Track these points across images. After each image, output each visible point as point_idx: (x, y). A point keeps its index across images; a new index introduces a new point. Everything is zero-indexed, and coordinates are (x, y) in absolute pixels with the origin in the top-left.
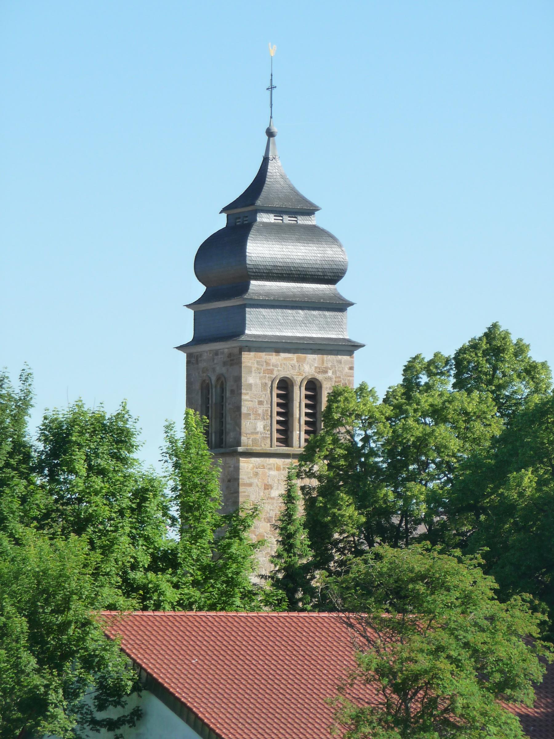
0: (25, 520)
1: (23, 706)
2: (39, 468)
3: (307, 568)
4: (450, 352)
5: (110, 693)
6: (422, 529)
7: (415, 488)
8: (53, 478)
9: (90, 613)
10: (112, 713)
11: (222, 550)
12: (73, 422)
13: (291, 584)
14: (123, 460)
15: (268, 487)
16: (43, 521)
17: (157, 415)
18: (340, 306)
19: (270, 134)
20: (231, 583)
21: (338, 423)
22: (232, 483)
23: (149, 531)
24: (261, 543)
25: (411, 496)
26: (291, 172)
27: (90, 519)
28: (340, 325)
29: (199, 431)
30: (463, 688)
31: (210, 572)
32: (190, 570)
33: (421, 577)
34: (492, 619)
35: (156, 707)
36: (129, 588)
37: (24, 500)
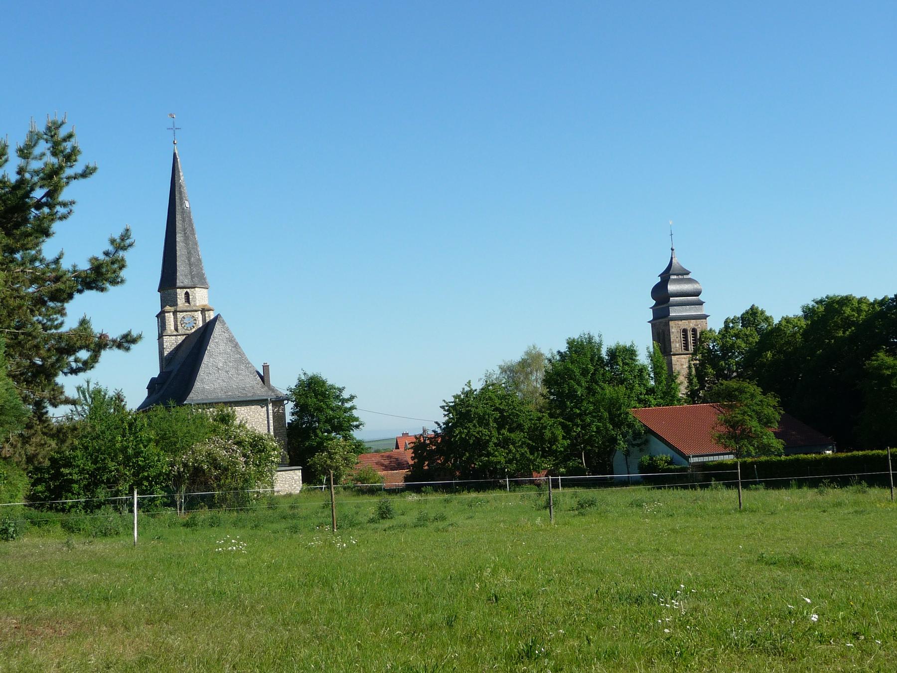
0: (604, 382)
2: (607, 365)
3: (698, 390)
4: (739, 315)
5: (637, 435)
6: (735, 374)
7: (732, 361)
8: (612, 367)
9: (628, 410)
10: (638, 441)
11: (669, 386)
12: (617, 349)
13: (693, 396)
14: (634, 360)
15: (682, 365)
16: (610, 382)
17: (644, 346)
18: (701, 303)
19: (672, 250)
20: (673, 397)
21: (704, 342)
22: (670, 364)
23: (644, 382)
24: (682, 383)
25: (144, 466)
26: (681, 261)
27: (625, 380)
29: (657, 348)
30: (754, 424)
32: (660, 394)
33: (736, 390)
34: (761, 401)
35: (654, 439)
36: (640, 401)
37: (603, 375)
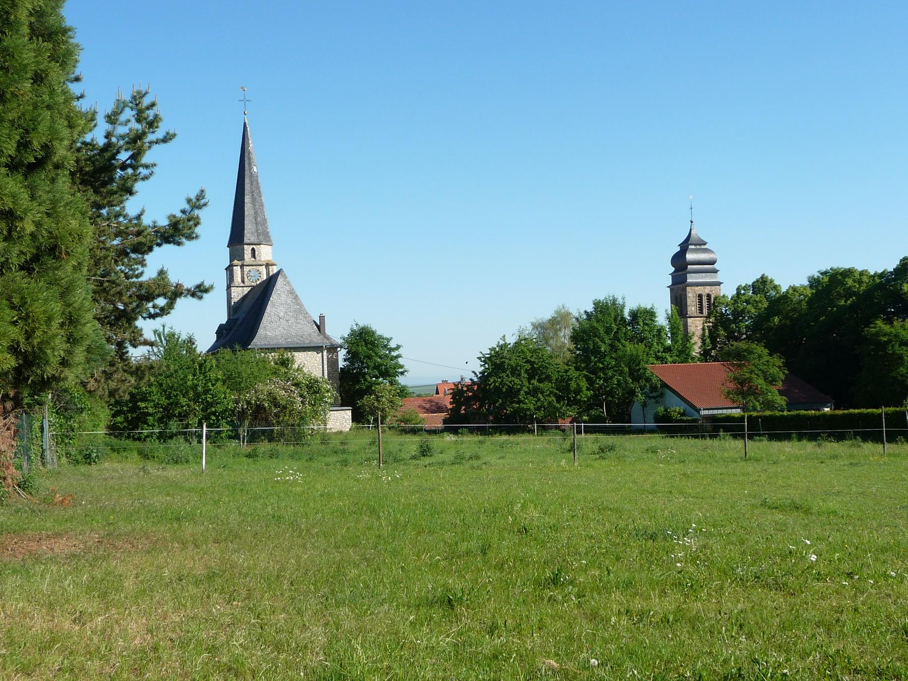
1: (628, 393)
5: (654, 388)
6: (744, 336)
10: (655, 394)
11: (684, 345)
12: (638, 311)
13: (705, 355)
17: (662, 308)
18: (716, 271)
20: (688, 355)
22: (686, 325)
24: (695, 343)
27: (645, 338)
28: (716, 277)
31: (681, 352)
33: (745, 350)
35: (668, 392)
36: (657, 358)
